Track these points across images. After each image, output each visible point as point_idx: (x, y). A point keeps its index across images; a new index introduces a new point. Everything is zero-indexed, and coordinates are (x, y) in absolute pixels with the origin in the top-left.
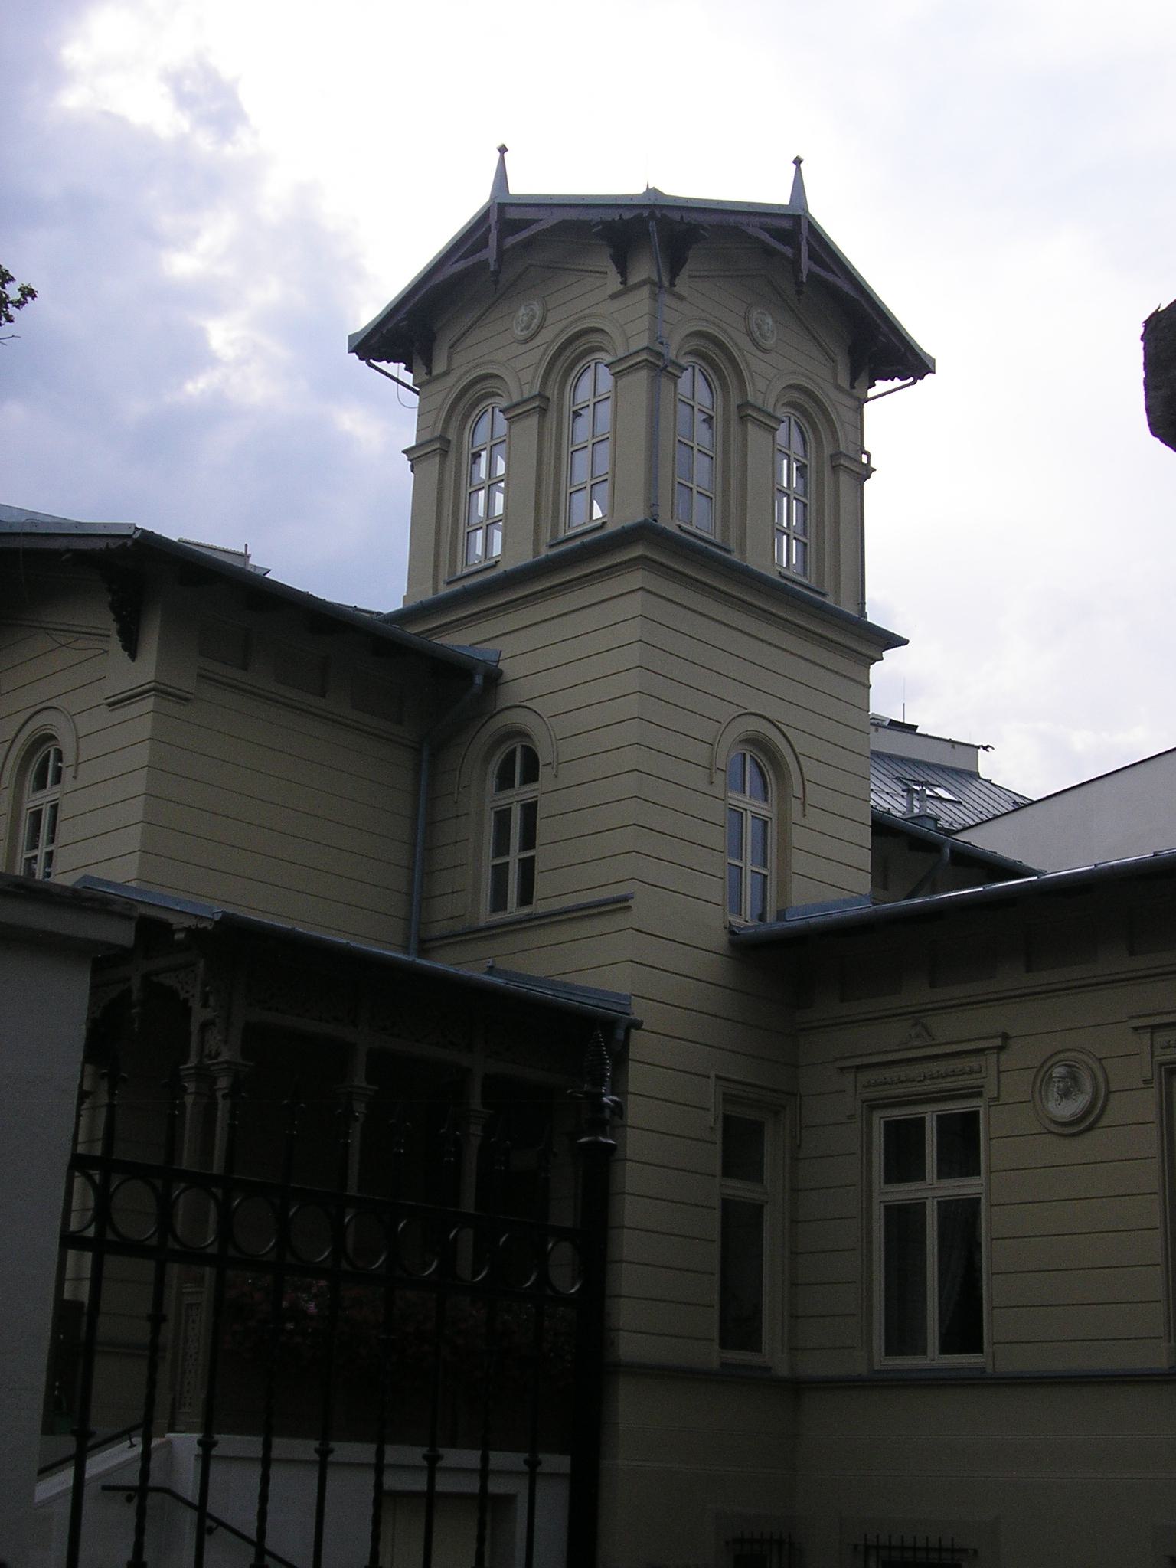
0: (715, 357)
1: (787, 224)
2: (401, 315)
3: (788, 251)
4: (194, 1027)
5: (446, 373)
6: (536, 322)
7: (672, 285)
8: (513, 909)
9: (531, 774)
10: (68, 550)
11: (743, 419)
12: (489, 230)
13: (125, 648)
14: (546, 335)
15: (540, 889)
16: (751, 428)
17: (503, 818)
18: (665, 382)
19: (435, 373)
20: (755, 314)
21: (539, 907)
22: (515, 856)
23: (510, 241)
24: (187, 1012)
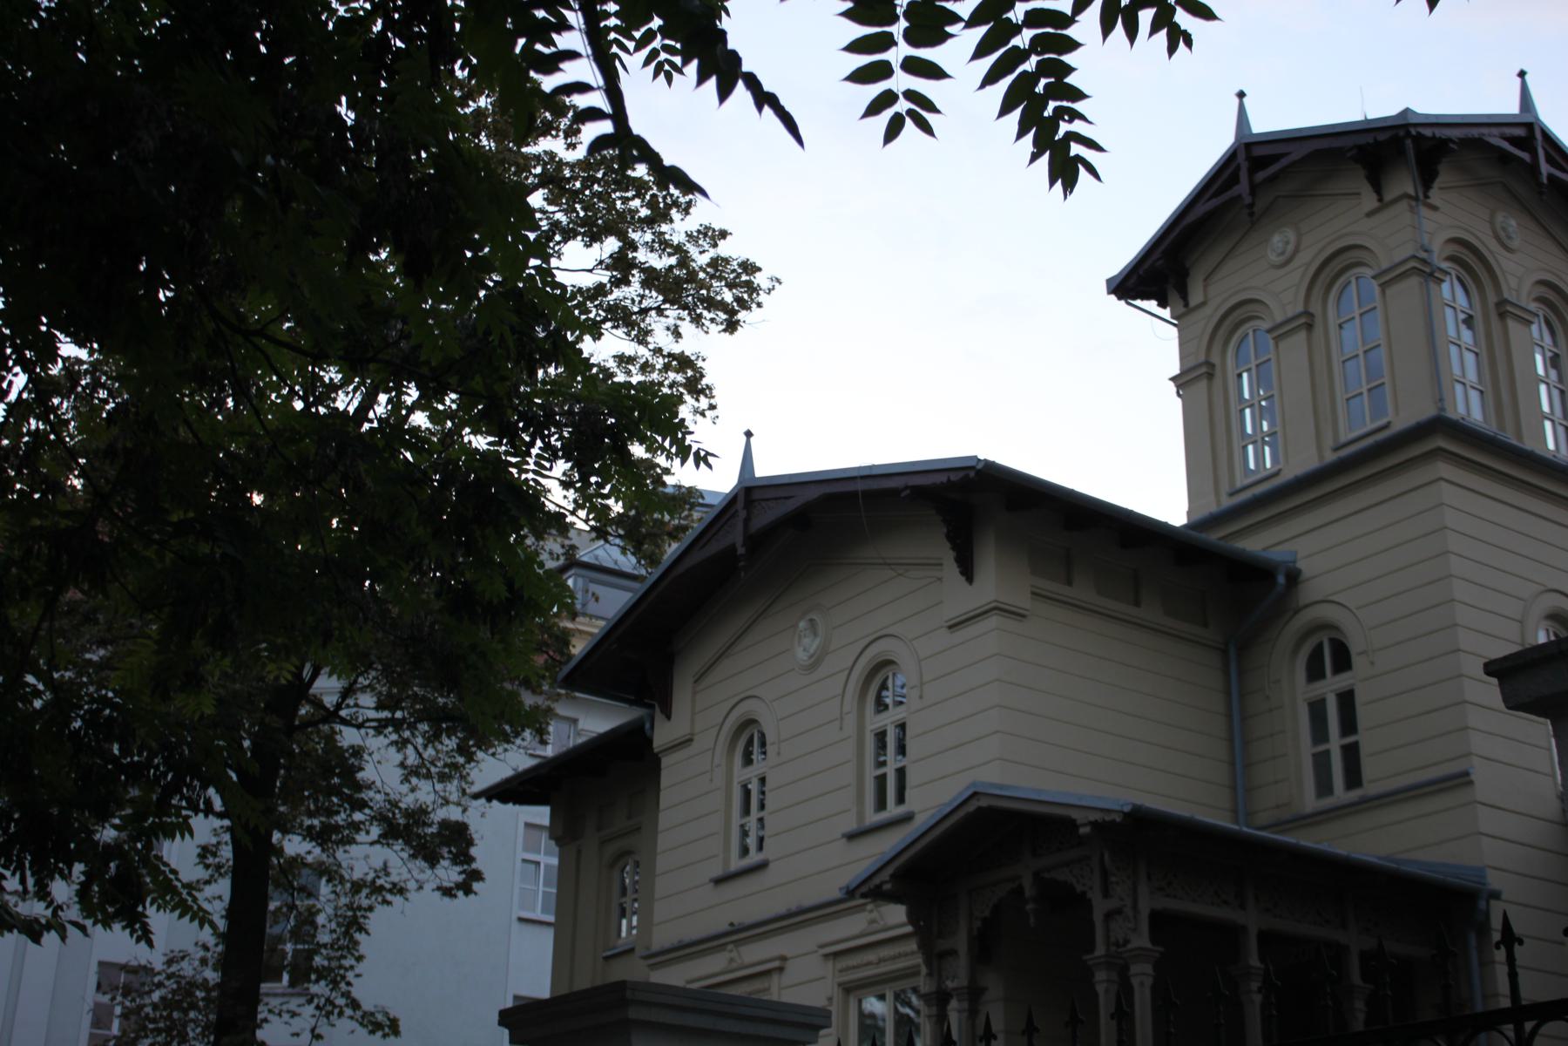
0: (1471, 263)
1: (1520, 132)
2: (1157, 254)
3: (1525, 156)
4: (1098, 917)
5: (1203, 304)
6: (1290, 248)
7: (1427, 197)
8: (1340, 794)
9: (1343, 661)
10: (906, 487)
11: (1502, 315)
12: (1238, 168)
13: (962, 573)
14: (1304, 257)
15: (1368, 769)
16: (1511, 323)
17: (1317, 710)
18: (1432, 285)
19: (1192, 303)
20: (1500, 218)
21: (1370, 788)
22: (1335, 743)
23: (1260, 176)
24: (1087, 905)
